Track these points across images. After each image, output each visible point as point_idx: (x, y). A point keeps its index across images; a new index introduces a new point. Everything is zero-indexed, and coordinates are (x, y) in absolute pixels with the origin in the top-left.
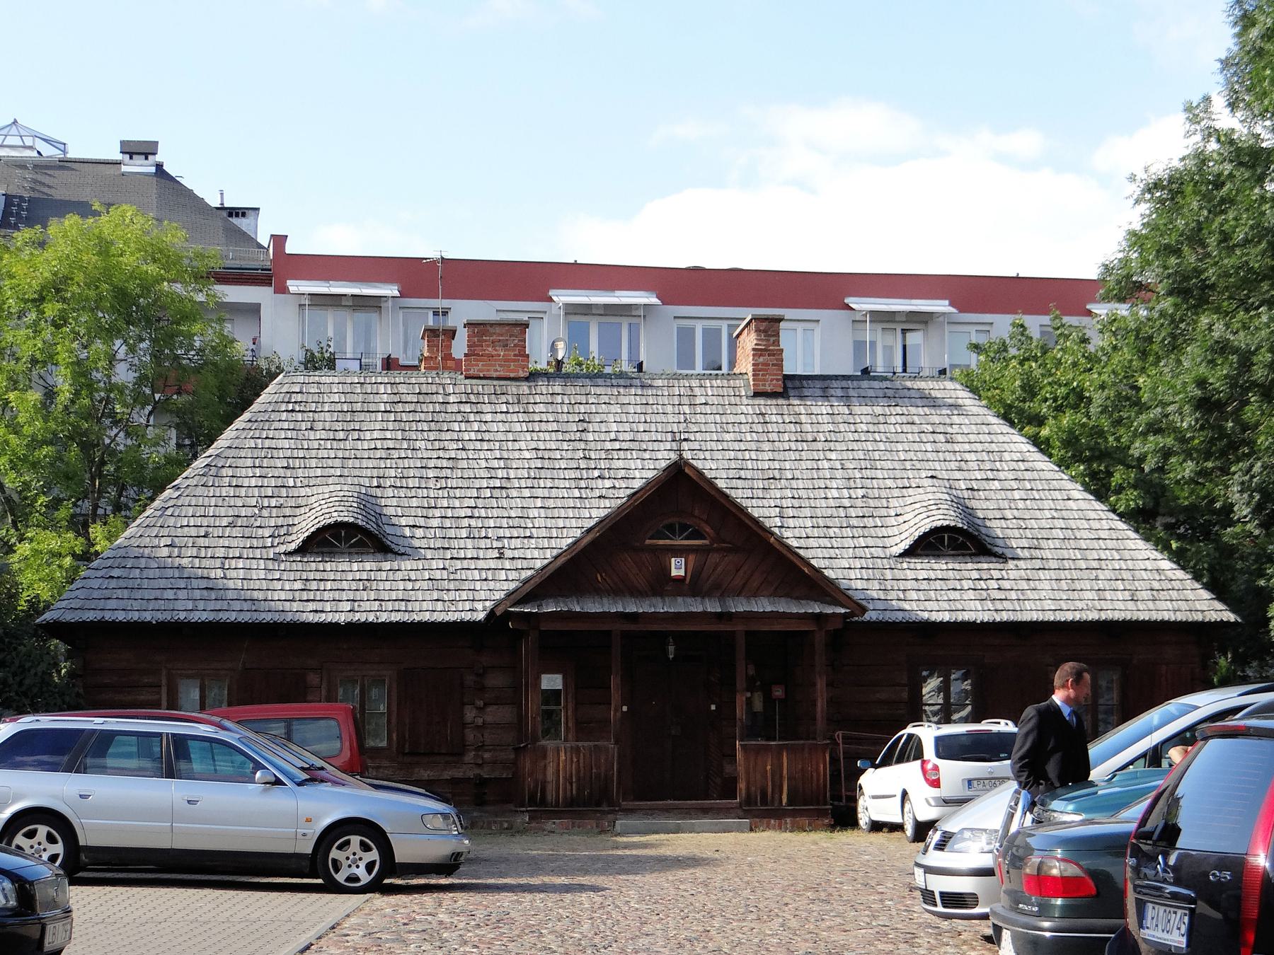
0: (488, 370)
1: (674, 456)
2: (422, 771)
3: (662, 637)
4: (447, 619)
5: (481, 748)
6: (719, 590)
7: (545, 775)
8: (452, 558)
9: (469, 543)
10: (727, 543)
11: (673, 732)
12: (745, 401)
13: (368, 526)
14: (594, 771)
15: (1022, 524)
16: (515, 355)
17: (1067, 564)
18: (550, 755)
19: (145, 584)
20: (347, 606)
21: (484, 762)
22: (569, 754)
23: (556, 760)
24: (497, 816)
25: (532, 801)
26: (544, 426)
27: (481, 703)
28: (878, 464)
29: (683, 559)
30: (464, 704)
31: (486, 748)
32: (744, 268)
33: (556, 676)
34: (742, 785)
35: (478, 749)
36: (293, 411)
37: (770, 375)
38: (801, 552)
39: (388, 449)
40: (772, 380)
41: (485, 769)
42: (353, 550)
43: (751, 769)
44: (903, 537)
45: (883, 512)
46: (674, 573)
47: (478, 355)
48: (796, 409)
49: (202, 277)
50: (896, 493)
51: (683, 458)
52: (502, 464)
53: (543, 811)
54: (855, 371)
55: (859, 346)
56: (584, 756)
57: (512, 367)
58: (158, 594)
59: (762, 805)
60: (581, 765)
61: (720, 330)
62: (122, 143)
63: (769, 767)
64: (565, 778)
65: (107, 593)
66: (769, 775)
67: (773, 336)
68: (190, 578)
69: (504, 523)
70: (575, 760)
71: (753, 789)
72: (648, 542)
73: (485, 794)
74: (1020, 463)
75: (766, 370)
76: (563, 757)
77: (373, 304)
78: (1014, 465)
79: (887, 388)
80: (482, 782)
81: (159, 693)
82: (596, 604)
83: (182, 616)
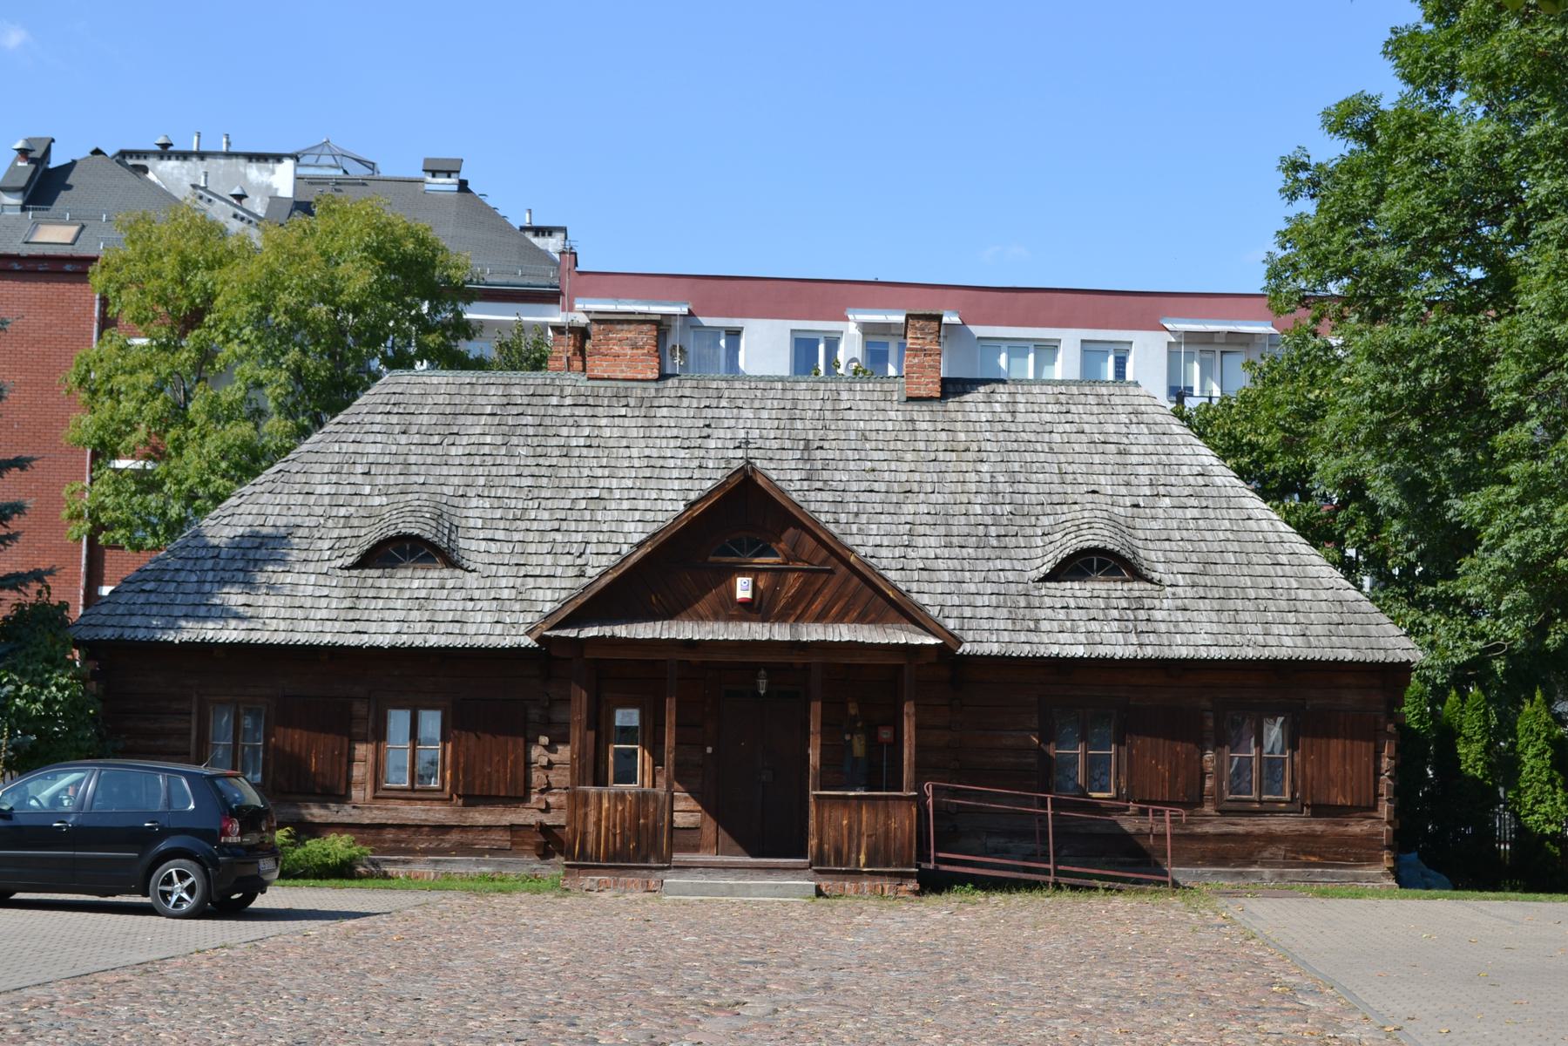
3: (754, 668)
4: (503, 644)
5: (548, 789)
8: (525, 576)
9: (549, 560)
12: (896, 406)
18: (593, 801)
20: (394, 627)
25: (568, 854)
26: (663, 432)
28: (1034, 477)
33: (630, 711)
34: (813, 842)
35: (542, 792)
36: (389, 413)
44: (1046, 559)
45: (1029, 531)
48: (953, 415)
50: (1048, 509)
52: (606, 472)
62: (427, 161)
64: (607, 829)
70: (620, 808)
71: (826, 846)
72: (711, 559)
74: (1199, 478)
76: (605, 805)
81: (190, 722)
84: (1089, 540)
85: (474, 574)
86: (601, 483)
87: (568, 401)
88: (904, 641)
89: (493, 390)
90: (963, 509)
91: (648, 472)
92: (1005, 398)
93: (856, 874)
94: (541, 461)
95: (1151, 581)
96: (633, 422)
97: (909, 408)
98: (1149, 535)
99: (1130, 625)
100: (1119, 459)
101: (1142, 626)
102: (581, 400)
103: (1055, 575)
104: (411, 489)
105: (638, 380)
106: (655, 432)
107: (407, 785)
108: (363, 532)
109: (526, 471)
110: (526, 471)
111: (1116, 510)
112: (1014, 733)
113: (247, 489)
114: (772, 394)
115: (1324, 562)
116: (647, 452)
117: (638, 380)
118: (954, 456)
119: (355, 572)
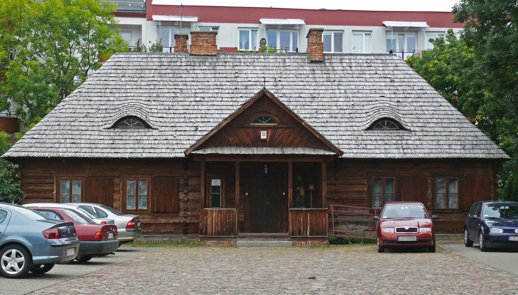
0: (200, 52)
1: (261, 88)
2: (161, 220)
6: (281, 145)
7: (207, 222)
10: (284, 124)
11: (267, 204)
12: (307, 64)
13: (141, 117)
14: (228, 220)
15: (419, 116)
16: (211, 46)
17: (437, 133)
18: (209, 214)
19: (48, 141)
21: (188, 216)
22: (217, 213)
23: (211, 216)
24: (192, 239)
25: (202, 233)
26: (221, 75)
27: (186, 191)
28: (361, 91)
29: (266, 132)
30: (179, 192)
31: (188, 210)
32: (328, 9)
35: (185, 210)
37: (317, 53)
38: (315, 128)
39: (155, 85)
40: (318, 56)
41: (188, 219)
42: (135, 127)
43: (294, 221)
44: (367, 122)
46: (262, 137)
47: (195, 46)
49: (109, 14)
51: (265, 89)
53: (206, 237)
54: (387, 52)
55: (388, 41)
56: (223, 214)
57: (210, 51)
58: (52, 145)
59: (298, 235)
60: (222, 218)
61: (330, 36)
63: (302, 219)
64: (215, 223)
65: (31, 145)
66: (302, 223)
67: (319, 37)
68: (66, 139)
69: (199, 116)
70: (220, 216)
72: (251, 124)
73: (188, 229)
75: (316, 52)
76: (214, 215)
77: (416, 30)
78: (418, 92)
79: (367, 59)
80: (186, 225)
81: (53, 186)
82: (229, 150)
83: (61, 154)
84: (384, 114)
85: (157, 130)
86: (199, 95)
87: (184, 64)
88: (323, 154)
89: (155, 60)
90: (335, 103)
91: (216, 91)
92: (347, 61)
93: (306, 239)
94: (176, 87)
95: (406, 130)
96: (208, 72)
97: (312, 65)
98: (404, 112)
99: (400, 146)
100: (391, 84)
101: (405, 146)
102: (189, 63)
103: (370, 128)
104: (129, 98)
105: (209, 55)
106: (217, 75)
107: (135, 208)
108: (113, 115)
109: (171, 91)
110: (171, 91)
111: (392, 103)
112: (358, 186)
113: (67, 99)
114: (260, 60)
115: (469, 122)
116: (216, 83)
117: (209, 55)
118: (329, 83)
119: (112, 130)
